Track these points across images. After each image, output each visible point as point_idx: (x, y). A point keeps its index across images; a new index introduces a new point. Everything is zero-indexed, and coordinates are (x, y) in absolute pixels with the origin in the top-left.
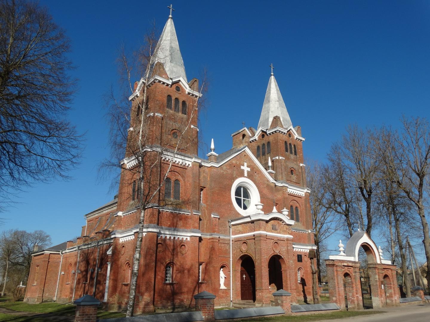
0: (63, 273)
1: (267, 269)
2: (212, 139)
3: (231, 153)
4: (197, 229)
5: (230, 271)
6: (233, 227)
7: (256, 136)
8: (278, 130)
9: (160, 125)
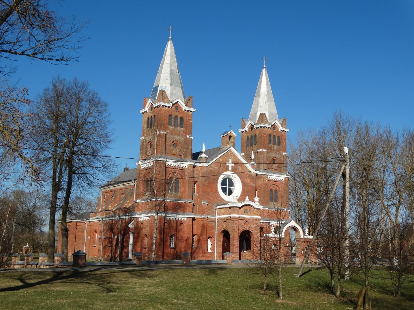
0: (89, 238)
1: (238, 240)
2: (204, 144)
3: (219, 153)
4: (191, 212)
5: (215, 241)
6: (219, 210)
7: (246, 127)
8: (262, 126)
9: (164, 140)
